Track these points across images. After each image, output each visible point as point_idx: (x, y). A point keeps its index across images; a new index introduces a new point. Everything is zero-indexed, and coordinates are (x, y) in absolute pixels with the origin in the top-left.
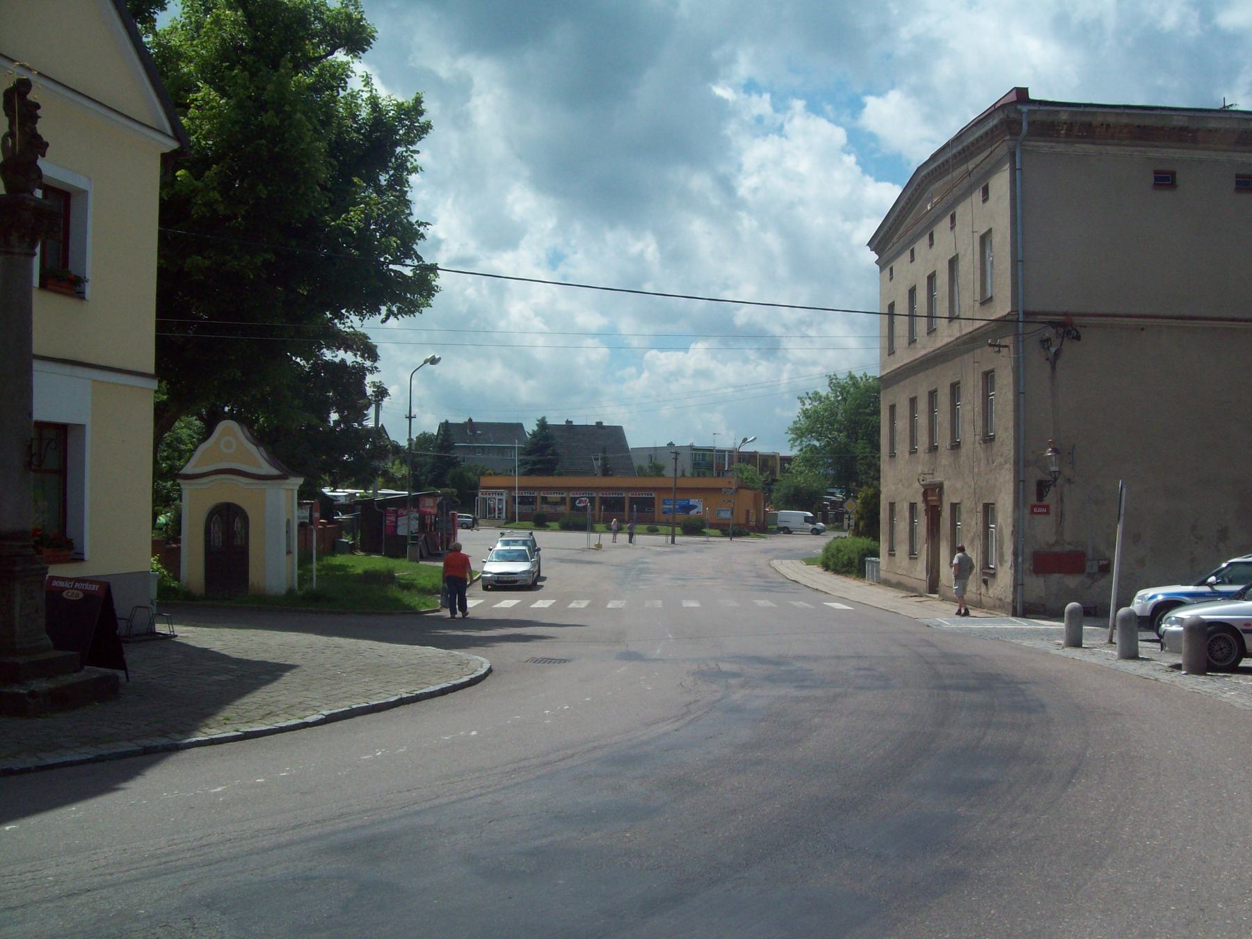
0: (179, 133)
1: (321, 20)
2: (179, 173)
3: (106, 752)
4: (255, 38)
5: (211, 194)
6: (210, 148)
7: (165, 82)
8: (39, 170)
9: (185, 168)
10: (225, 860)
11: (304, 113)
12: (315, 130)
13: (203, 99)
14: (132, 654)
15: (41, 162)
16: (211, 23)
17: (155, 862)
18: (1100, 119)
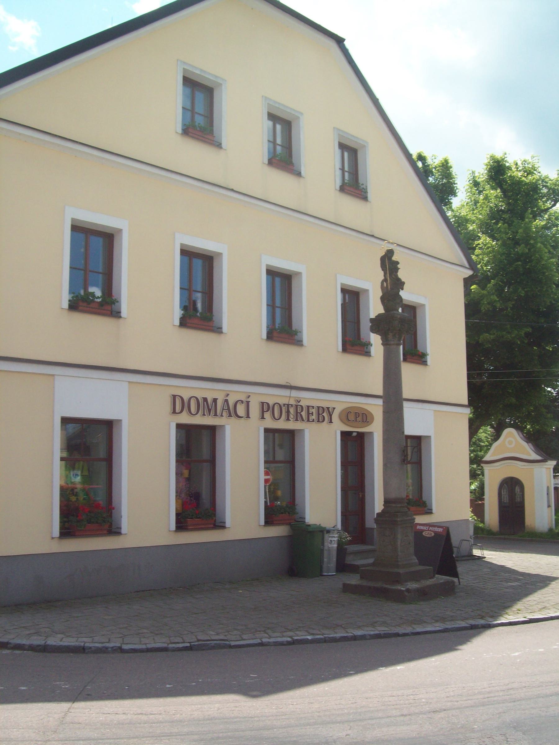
0: (472, 265)
1: (546, 187)
2: (472, 287)
3: (450, 627)
4: (508, 204)
5: (492, 297)
6: (489, 271)
7: (462, 237)
8: (401, 297)
9: (476, 284)
10: (523, 699)
11: (542, 243)
12: (549, 252)
13: (483, 243)
14: (461, 568)
15: (402, 293)
16: (483, 199)
17: (482, 696)
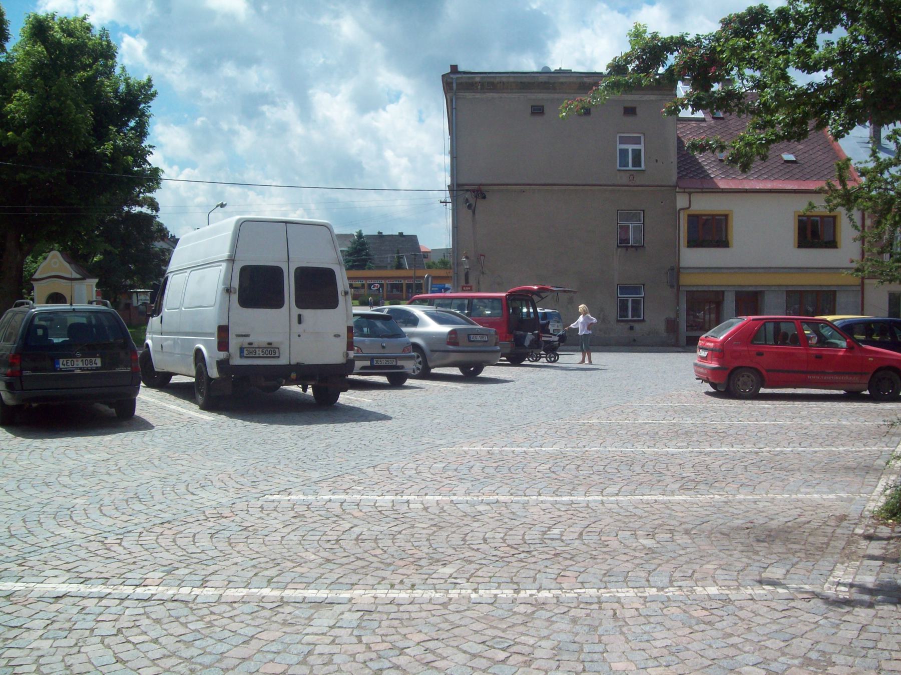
18: (498, 80)
